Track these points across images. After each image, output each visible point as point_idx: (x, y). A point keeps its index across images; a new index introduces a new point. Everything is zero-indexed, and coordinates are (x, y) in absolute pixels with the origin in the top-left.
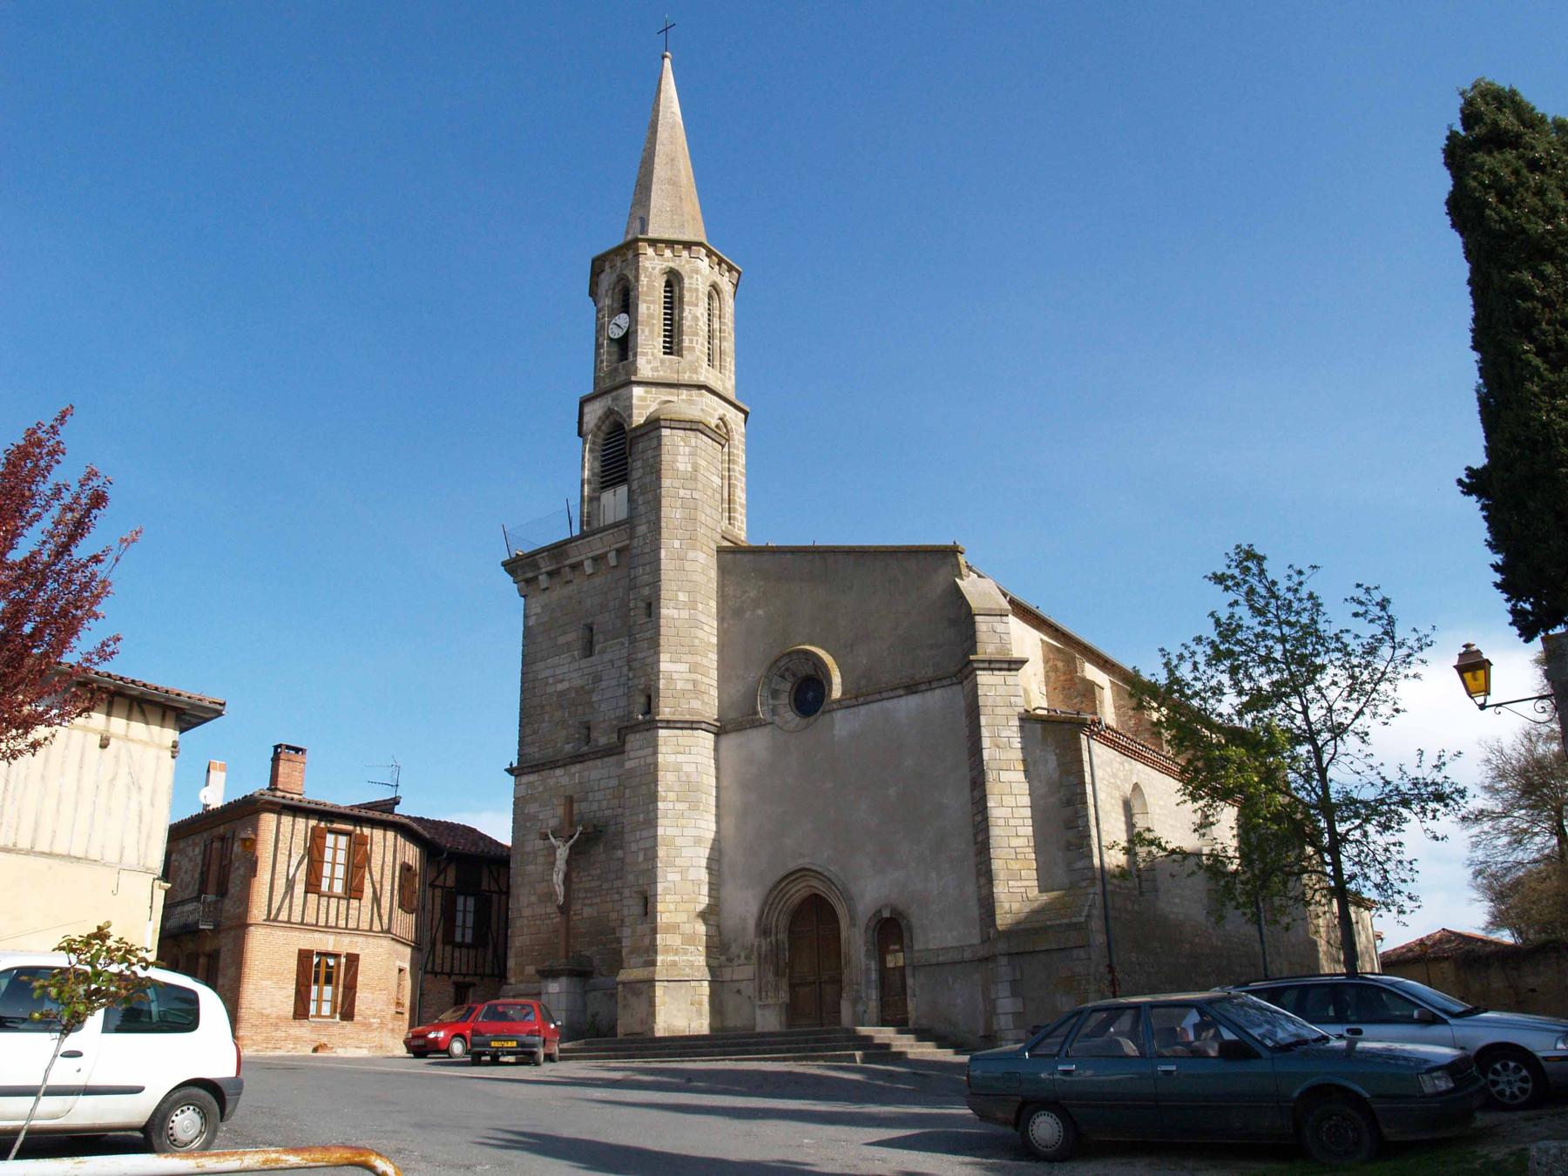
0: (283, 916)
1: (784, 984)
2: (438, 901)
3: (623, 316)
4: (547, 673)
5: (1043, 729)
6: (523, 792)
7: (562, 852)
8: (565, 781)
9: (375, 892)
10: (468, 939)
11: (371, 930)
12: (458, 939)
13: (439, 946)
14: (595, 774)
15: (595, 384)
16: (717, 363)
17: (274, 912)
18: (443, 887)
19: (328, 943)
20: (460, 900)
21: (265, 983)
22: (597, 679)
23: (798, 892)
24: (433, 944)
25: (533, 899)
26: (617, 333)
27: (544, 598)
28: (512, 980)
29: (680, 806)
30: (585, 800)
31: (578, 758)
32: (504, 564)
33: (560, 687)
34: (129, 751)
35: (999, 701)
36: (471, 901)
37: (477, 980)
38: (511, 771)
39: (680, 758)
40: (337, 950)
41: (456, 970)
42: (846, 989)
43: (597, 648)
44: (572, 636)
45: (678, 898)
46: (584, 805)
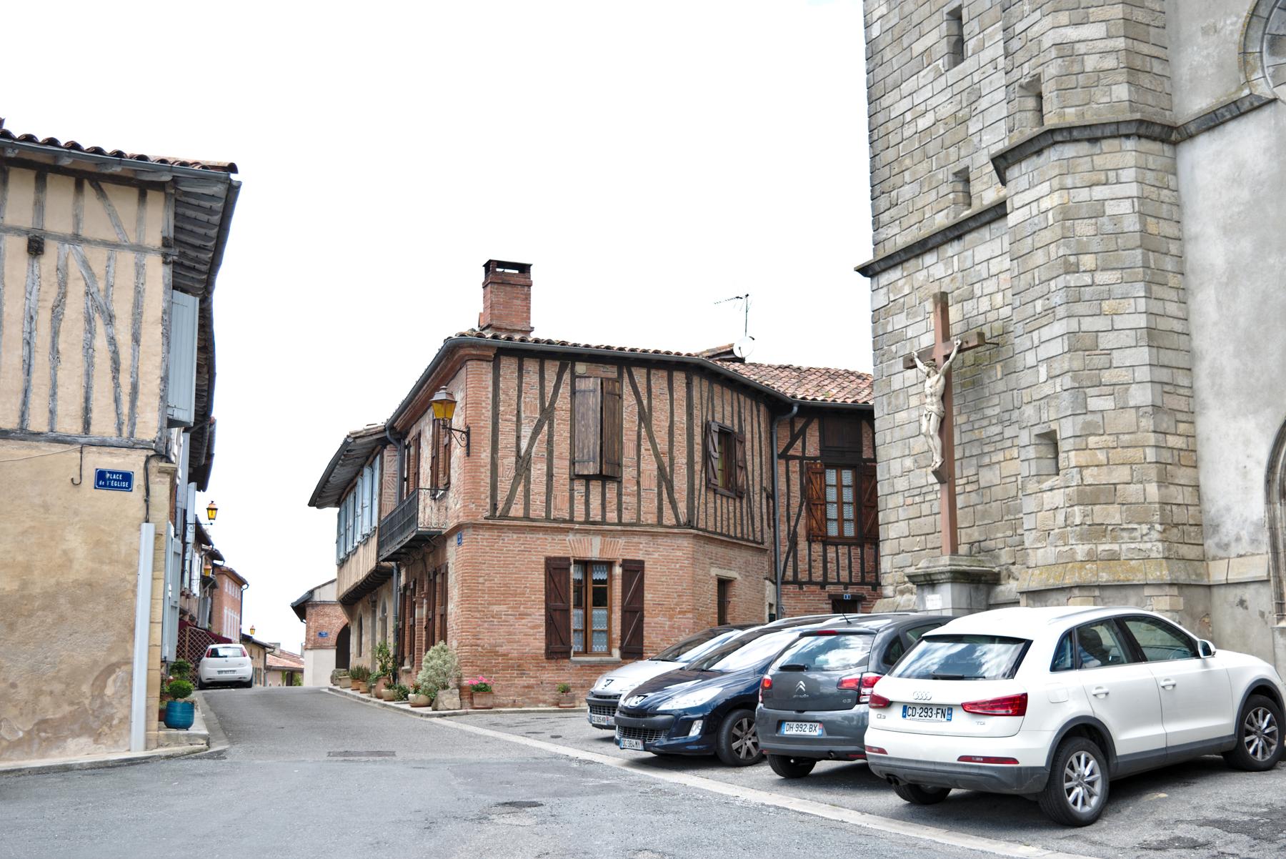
0: (517, 510)
2: (795, 478)
4: (905, 104)
6: (882, 300)
7: (935, 383)
8: (939, 271)
9: (661, 468)
10: (850, 531)
11: (660, 523)
12: (833, 530)
13: (802, 545)
14: (982, 252)
17: (500, 506)
18: (802, 458)
19: (593, 548)
20: (831, 476)
21: (496, 608)
25: (909, 463)
28: (888, 591)
29: (1101, 277)
31: (956, 232)
33: (923, 123)
34: (86, 264)
36: (847, 477)
38: (865, 270)
39: (1099, 193)
40: (607, 556)
41: (832, 576)
43: (970, 45)
44: (935, 37)
45: (1109, 440)
46: (968, 306)
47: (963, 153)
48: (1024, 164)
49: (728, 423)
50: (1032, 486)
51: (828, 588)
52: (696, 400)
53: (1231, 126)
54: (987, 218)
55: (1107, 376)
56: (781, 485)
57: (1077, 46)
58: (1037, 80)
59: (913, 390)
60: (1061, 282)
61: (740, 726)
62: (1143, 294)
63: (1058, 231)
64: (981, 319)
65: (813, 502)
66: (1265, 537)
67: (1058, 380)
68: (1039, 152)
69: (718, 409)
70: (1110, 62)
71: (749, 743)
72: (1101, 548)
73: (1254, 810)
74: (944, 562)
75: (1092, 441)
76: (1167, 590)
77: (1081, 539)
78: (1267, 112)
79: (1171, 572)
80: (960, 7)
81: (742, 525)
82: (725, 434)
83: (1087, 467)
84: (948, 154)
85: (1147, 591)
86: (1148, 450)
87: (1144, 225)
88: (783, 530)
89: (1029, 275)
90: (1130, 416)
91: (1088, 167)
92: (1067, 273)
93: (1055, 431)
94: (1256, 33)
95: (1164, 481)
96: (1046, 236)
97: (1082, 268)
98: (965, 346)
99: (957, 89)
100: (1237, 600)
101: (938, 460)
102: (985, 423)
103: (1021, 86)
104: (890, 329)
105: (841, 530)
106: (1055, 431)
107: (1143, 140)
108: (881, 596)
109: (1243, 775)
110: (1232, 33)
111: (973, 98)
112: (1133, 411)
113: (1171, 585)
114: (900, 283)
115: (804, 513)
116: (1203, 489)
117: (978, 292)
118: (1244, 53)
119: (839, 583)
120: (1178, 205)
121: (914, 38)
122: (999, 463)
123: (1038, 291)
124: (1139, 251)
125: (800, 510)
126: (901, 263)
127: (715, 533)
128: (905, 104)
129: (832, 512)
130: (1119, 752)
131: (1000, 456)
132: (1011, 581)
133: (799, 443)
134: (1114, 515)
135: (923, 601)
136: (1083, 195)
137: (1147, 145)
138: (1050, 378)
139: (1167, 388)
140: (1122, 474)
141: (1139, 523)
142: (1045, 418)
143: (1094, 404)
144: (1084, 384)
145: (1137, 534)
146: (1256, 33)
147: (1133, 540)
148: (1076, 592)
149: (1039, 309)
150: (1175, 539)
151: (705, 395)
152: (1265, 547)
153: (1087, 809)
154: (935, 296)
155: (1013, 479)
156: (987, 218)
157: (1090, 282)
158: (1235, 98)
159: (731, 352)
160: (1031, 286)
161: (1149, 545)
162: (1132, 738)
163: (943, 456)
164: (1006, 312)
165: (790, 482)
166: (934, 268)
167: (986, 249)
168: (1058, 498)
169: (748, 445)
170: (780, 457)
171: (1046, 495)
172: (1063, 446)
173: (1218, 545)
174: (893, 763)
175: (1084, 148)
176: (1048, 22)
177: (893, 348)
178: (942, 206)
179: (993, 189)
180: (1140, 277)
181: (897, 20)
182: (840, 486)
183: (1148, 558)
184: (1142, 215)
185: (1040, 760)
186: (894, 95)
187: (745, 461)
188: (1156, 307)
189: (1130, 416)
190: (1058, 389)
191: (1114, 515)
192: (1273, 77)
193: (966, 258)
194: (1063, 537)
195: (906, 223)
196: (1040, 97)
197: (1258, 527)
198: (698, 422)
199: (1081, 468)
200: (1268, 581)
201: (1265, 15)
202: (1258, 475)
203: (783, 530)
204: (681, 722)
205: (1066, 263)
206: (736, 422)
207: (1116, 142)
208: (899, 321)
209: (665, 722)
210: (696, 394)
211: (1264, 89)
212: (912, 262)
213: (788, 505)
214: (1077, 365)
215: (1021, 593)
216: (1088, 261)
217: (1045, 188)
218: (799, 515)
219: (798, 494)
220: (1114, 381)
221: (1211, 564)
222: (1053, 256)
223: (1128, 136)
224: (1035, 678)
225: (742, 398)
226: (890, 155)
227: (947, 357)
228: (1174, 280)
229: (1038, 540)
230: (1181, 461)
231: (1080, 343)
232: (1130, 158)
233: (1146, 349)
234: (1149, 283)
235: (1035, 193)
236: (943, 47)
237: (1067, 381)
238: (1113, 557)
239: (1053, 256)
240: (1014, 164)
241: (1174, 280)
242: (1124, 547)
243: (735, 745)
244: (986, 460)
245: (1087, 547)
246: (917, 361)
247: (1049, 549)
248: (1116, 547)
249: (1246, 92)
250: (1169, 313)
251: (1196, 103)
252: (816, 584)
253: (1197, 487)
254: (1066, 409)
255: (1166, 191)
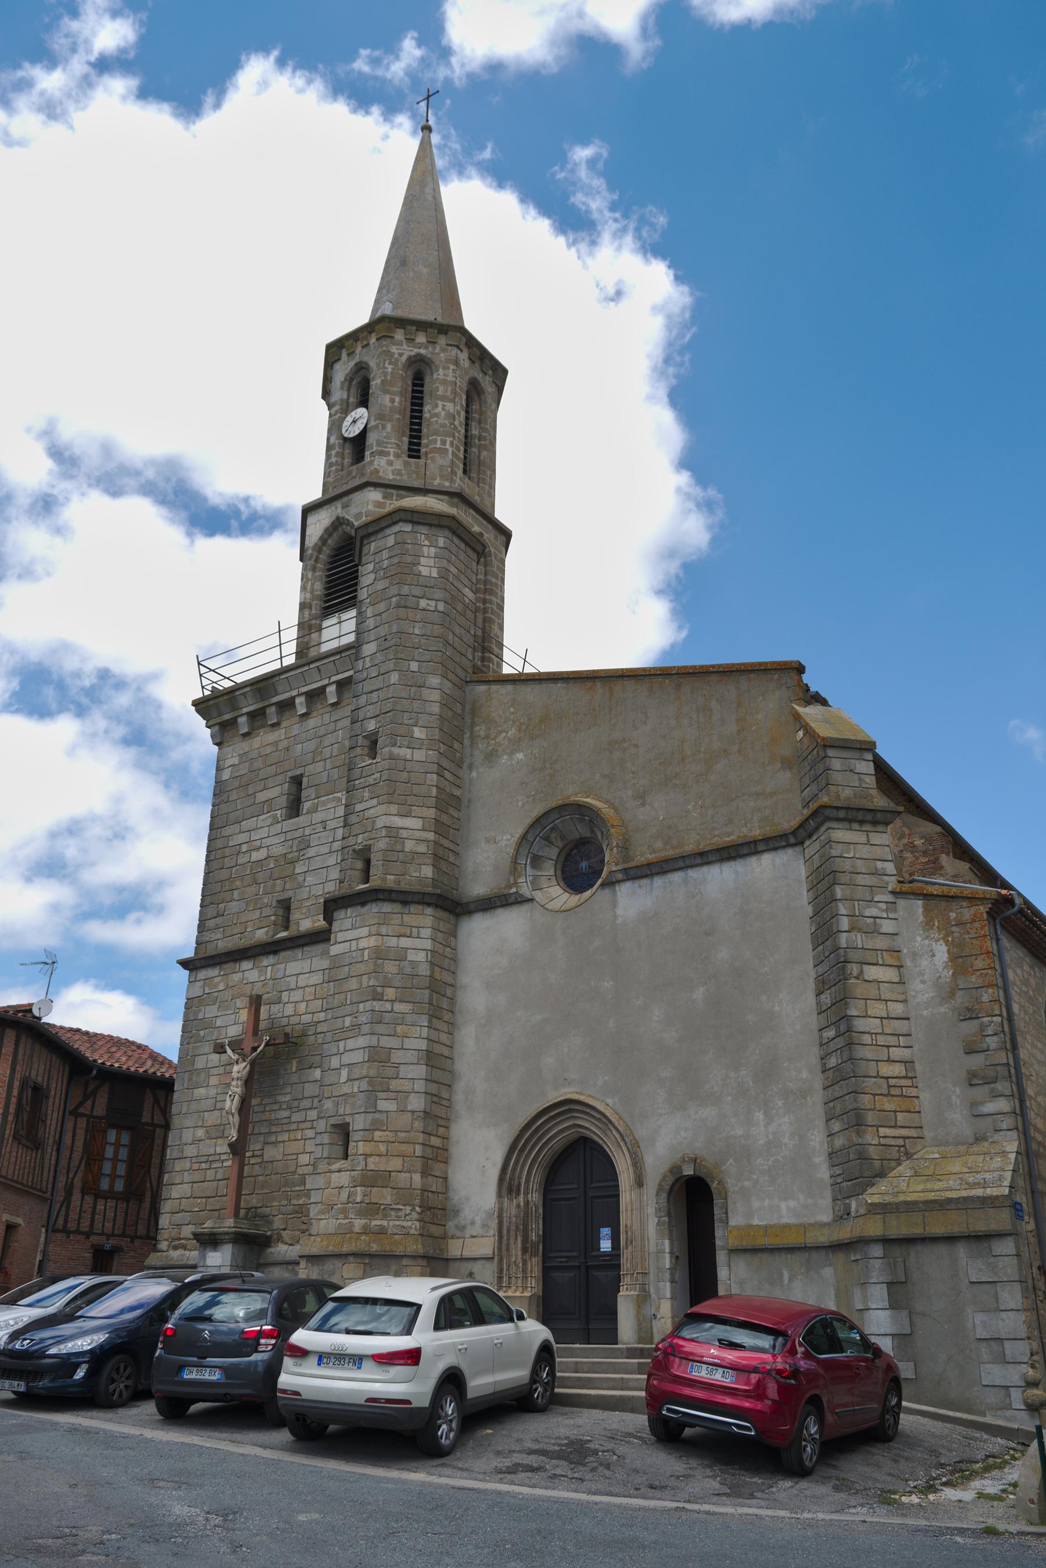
1: (535, 1265)
2: (81, 1134)
3: (362, 411)
4: (243, 838)
5: (927, 910)
6: (197, 991)
7: (240, 1069)
10: (119, 1186)
12: (105, 1184)
13: (76, 1196)
14: (293, 967)
15: (324, 491)
16: (474, 475)
18: (89, 1117)
20: (112, 1136)
22: (305, 844)
23: (559, 1134)
24: (69, 1194)
25: (200, 1133)
26: (352, 431)
27: (244, 746)
28: (163, 1245)
29: (399, 1007)
30: (279, 1001)
31: (273, 948)
32: (196, 704)
33: (256, 856)
35: (860, 866)
36: (125, 1138)
37: (124, 1243)
38: (185, 964)
39: (404, 942)
41: (98, 1227)
42: (626, 1280)
43: (306, 806)
44: (277, 792)
46: (275, 1008)
47: (288, 886)
48: (349, 910)
49: (40, 1079)
50: (322, 1167)
51: (94, 1239)
52: (20, 1057)
53: (499, 911)
54: (302, 941)
55: (394, 1085)
56: (67, 1140)
57: (401, 831)
58: (367, 849)
59: (215, 1071)
60: (368, 1005)
61: (118, 1370)
62: (426, 1024)
63: (371, 967)
64: (285, 1021)
65: (92, 1157)
66: (494, 1224)
67: (357, 1083)
68: (363, 904)
69: (35, 1066)
70: (422, 848)
71: (122, 1386)
72: (374, 1223)
73: (558, 1441)
74: (229, 1224)
75: (377, 1134)
76: (420, 1261)
77: (359, 1215)
78: (525, 908)
79: (424, 1247)
80: (302, 775)
81: (34, 1174)
82: (37, 1089)
83: (371, 1155)
84: (274, 886)
85: (405, 1262)
86: (417, 1147)
87: (432, 971)
88: (62, 1179)
89: (342, 996)
90: (407, 1118)
91: (399, 921)
92: (374, 1000)
93: (348, 1124)
94: (524, 851)
95: (425, 1173)
96: (361, 968)
97: (385, 998)
98: (272, 1042)
99: (289, 836)
100: (467, 1273)
101: (234, 1135)
102: (276, 1107)
103: (354, 850)
104: (201, 1016)
105: (112, 1185)
106: (348, 1124)
107: (438, 910)
108: (155, 1250)
109: (531, 1415)
110: (506, 846)
111: (303, 847)
112: (410, 1114)
113: (423, 1257)
114: (217, 980)
115: (82, 1167)
116: (450, 1180)
117: (285, 999)
118: (515, 862)
119: (102, 1234)
120: (455, 960)
121: (259, 789)
122: (284, 1142)
123: (348, 1009)
124: (427, 991)
125: (80, 1164)
126: (220, 964)
127: (12, 1180)
128: (243, 838)
129: (107, 1167)
130: (469, 1397)
131: (286, 1137)
132: (280, 1245)
133: (89, 1102)
134: (386, 1197)
135: (204, 1257)
136: (393, 942)
137: (441, 913)
138: (349, 1080)
139: (435, 1099)
140: (396, 1164)
141: (404, 1205)
142: (341, 1111)
143: (382, 1105)
144: (377, 1088)
145: (402, 1214)
146: (524, 851)
147: (398, 1218)
148: (351, 1259)
149: (347, 1023)
150: (427, 1220)
151: (28, 1052)
152: (493, 1230)
153: (448, 1442)
154: (251, 997)
155: (295, 1157)
156: (302, 941)
157: (390, 1009)
158: (506, 892)
159: (30, 1011)
160: (343, 1005)
161: (409, 1224)
162: (480, 1384)
163: (239, 1131)
164: (306, 1019)
165: (76, 1138)
166: (249, 973)
167: (301, 970)
168: (344, 1179)
169: (51, 1100)
170: (71, 1113)
171: (333, 1175)
172: (354, 1136)
173: (457, 1227)
174: (306, 1404)
175: (397, 907)
176: (381, 809)
177: (202, 1033)
178: (263, 924)
179: (310, 919)
180: (426, 1011)
181: (246, 771)
182: (117, 1145)
183: (408, 1234)
184: (432, 964)
185: (425, 1402)
186: (235, 828)
187: (46, 1115)
188: (434, 1035)
189: (407, 1118)
190: (356, 1090)
191: (386, 1197)
192: (532, 883)
193: (278, 969)
194: (344, 1212)
195: (228, 932)
196: (368, 862)
197: (490, 1215)
198: (18, 1076)
199: (366, 1156)
200: (493, 1258)
201: (531, 840)
202: (494, 1174)
203: (62, 1179)
204: (69, 1363)
205: (374, 991)
206: (46, 1079)
207: (420, 907)
208: (210, 1012)
209: (52, 1364)
210: (21, 1051)
211: (526, 890)
212: (230, 965)
213: (70, 1158)
214: (372, 1073)
215: (300, 1257)
216: (390, 993)
217: (365, 931)
218: (79, 1167)
219: (81, 1149)
220: (399, 1089)
221: (450, 1241)
222: (365, 984)
223: (429, 905)
224: (423, 1336)
225: (54, 1058)
226: (224, 874)
227: (254, 1049)
228: (447, 1016)
229: (322, 1212)
230: (436, 1158)
231: (378, 1056)
232: (429, 921)
233: (424, 1067)
234: (432, 1016)
235: (356, 934)
236: (283, 801)
237: (364, 1085)
238: (382, 1231)
239: (365, 984)
240: (341, 908)
241: (447, 1016)
242: (391, 1223)
243: (112, 1387)
244: (273, 1138)
245: (363, 1221)
246: (227, 1048)
247: (330, 1220)
248: (385, 1223)
249: (514, 890)
250: (441, 1041)
251: (478, 888)
252: (82, 1233)
253: (445, 1179)
254: (360, 1107)
255: (448, 949)
